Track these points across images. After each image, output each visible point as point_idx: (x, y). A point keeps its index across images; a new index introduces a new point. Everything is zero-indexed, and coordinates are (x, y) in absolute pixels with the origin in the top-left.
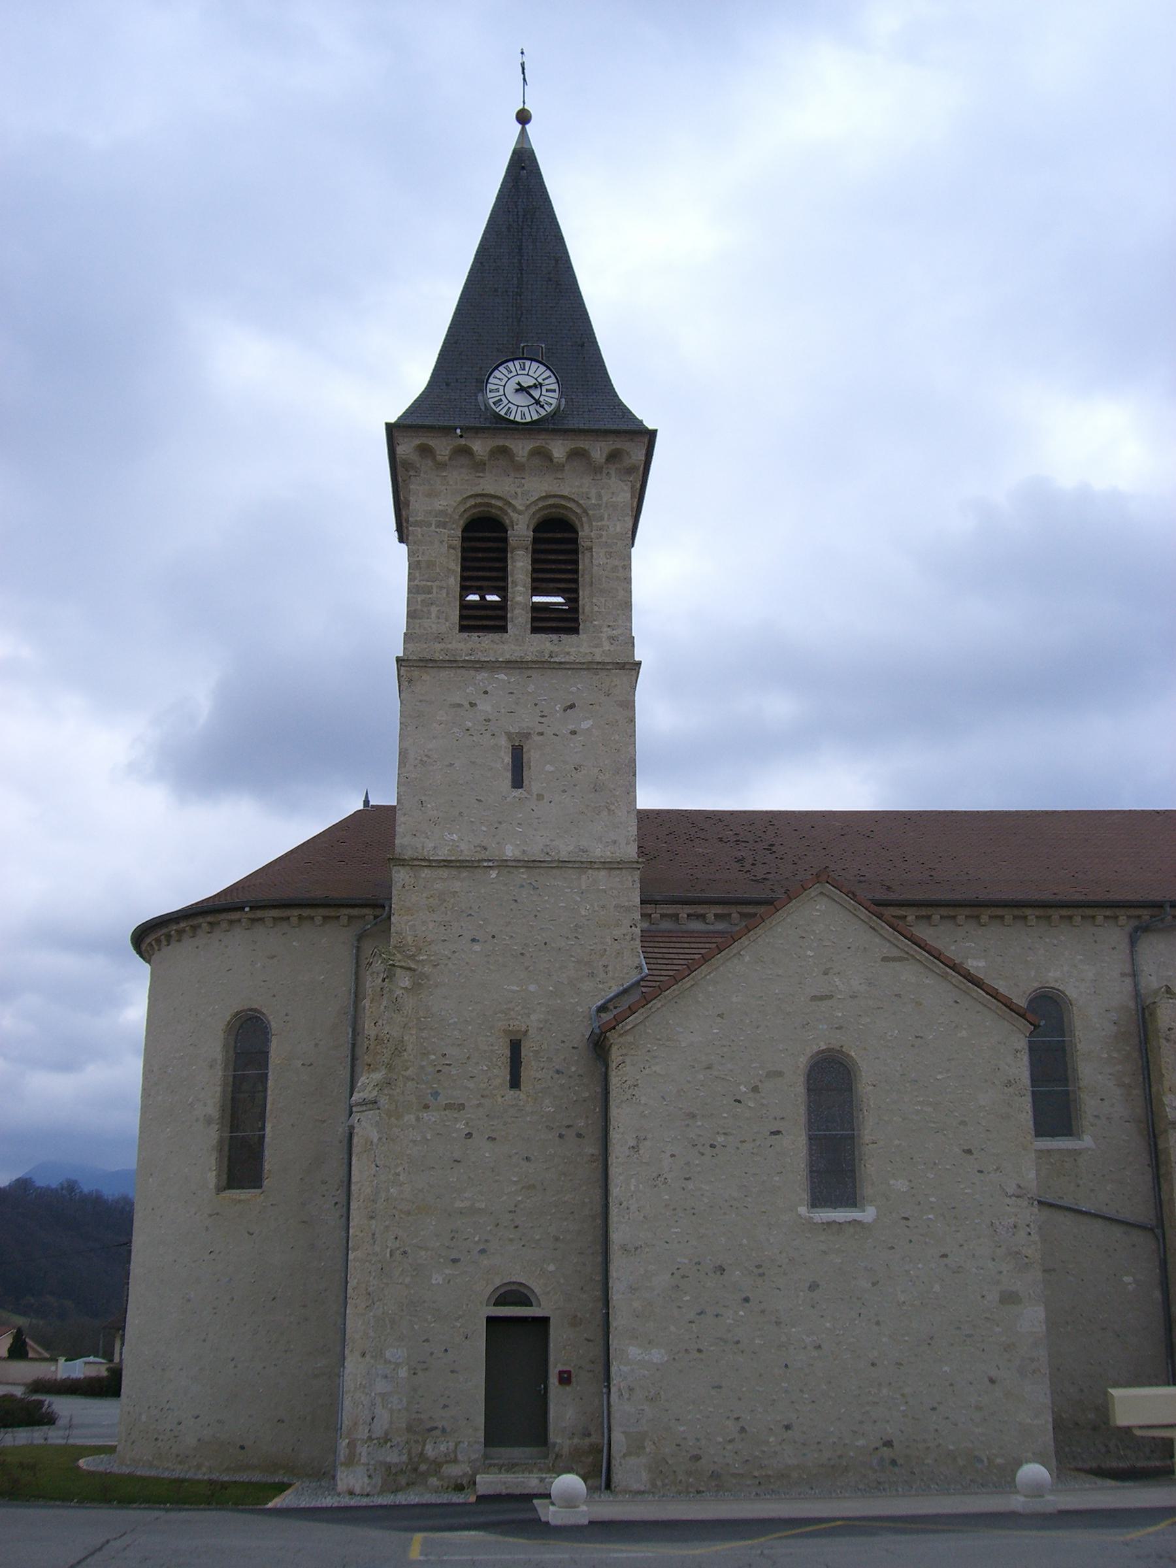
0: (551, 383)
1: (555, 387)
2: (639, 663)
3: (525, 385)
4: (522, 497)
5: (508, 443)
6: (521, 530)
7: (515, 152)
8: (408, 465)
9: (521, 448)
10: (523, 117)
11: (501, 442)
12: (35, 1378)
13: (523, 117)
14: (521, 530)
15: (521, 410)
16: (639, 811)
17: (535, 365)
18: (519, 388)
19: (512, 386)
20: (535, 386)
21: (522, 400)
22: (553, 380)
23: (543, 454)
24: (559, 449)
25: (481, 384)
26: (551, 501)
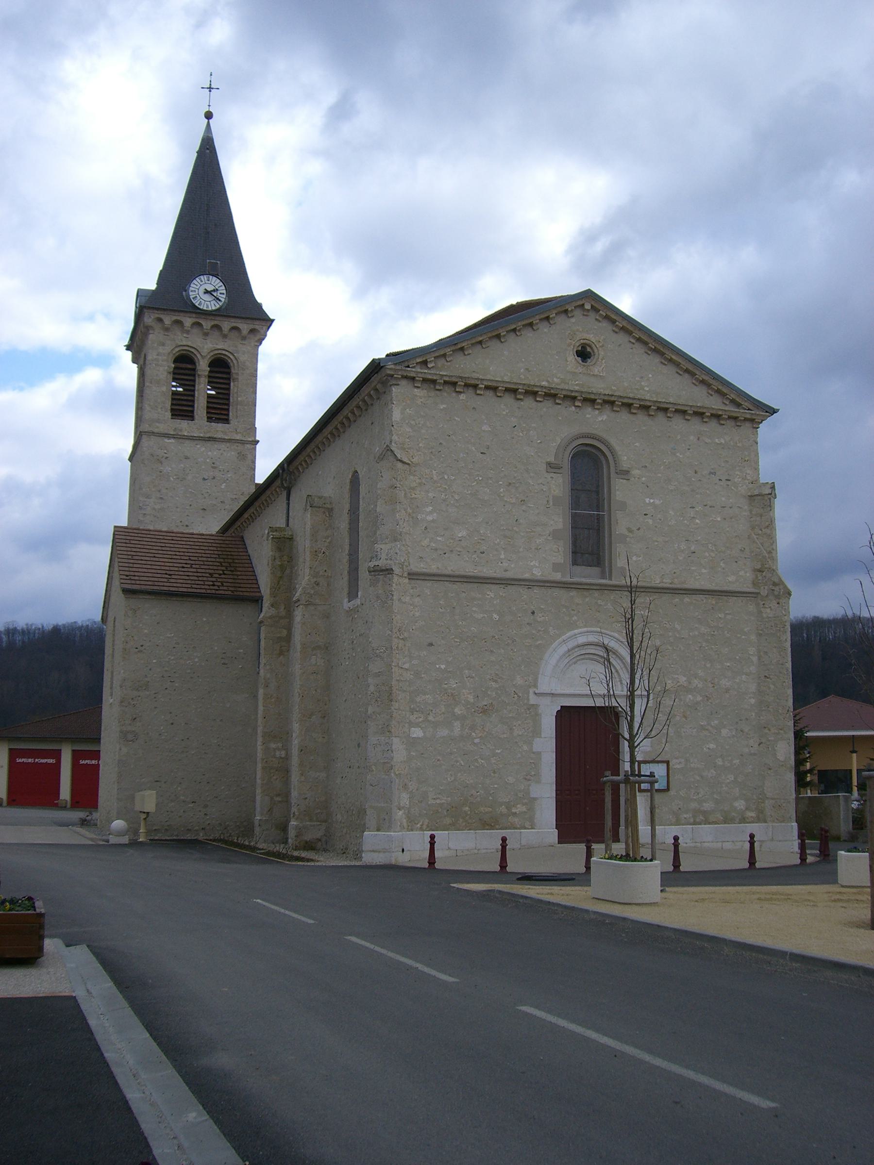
0: (222, 289)
1: (224, 292)
2: (258, 441)
3: (209, 290)
4: (205, 347)
5: (162, 316)
6: (203, 366)
7: (203, 140)
8: (148, 328)
9: (207, 324)
10: (209, 116)
11: (216, 322)
12: (55, 623)
13: (209, 116)
14: (203, 366)
15: (208, 304)
16: (257, 484)
17: (215, 278)
18: (205, 291)
19: (202, 290)
20: (214, 291)
21: (207, 297)
22: (224, 288)
23: (217, 327)
24: (226, 325)
25: (185, 288)
26: (217, 352)
